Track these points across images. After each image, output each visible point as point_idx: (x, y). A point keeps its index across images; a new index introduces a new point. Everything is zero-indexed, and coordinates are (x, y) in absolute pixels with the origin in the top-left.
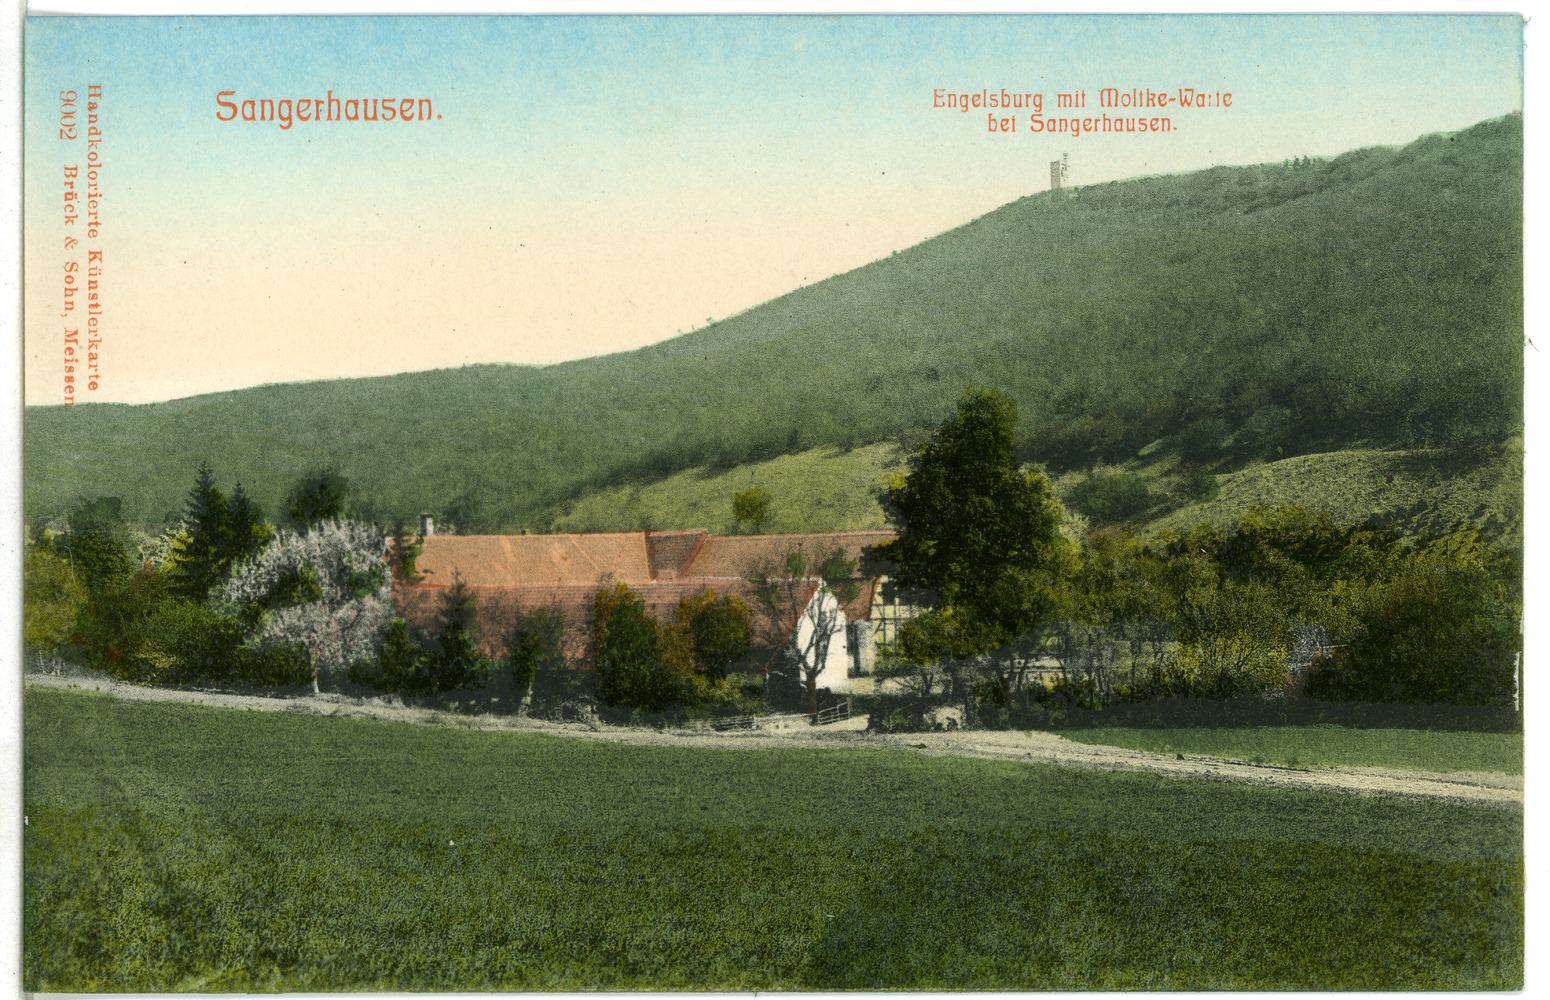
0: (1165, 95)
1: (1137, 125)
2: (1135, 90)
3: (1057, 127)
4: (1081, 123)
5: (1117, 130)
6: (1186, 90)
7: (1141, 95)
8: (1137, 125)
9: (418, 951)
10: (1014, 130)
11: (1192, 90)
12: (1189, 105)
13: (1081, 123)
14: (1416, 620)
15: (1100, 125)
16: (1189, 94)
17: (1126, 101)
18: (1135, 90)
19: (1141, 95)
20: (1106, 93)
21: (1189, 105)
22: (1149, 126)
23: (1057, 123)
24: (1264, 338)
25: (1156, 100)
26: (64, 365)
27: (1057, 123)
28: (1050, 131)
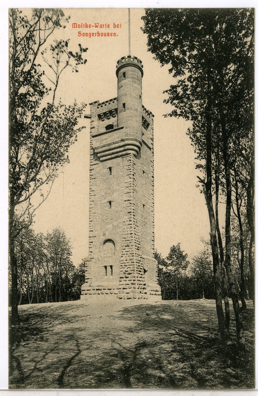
0: (91, 25)
1: (107, 35)
2: (82, 23)
3: (102, 27)
4: (91, 34)
5: (104, 36)
6: (97, 23)
7: (84, 25)
8: (107, 35)
9: (16, 373)
10: (121, 27)
11: (98, 24)
12: (97, 27)
13: (91, 34)
14: (194, 136)
15: (97, 35)
16: (98, 25)
17: (79, 26)
18: (82, 23)
19: (84, 25)
20: (74, 25)
21: (97, 27)
22: (110, 35)
23: (85, 34)
24: (60, 25)
25: (88, 26)
26: (85, 28)
27: (85, 34)
28: (76, 24)
